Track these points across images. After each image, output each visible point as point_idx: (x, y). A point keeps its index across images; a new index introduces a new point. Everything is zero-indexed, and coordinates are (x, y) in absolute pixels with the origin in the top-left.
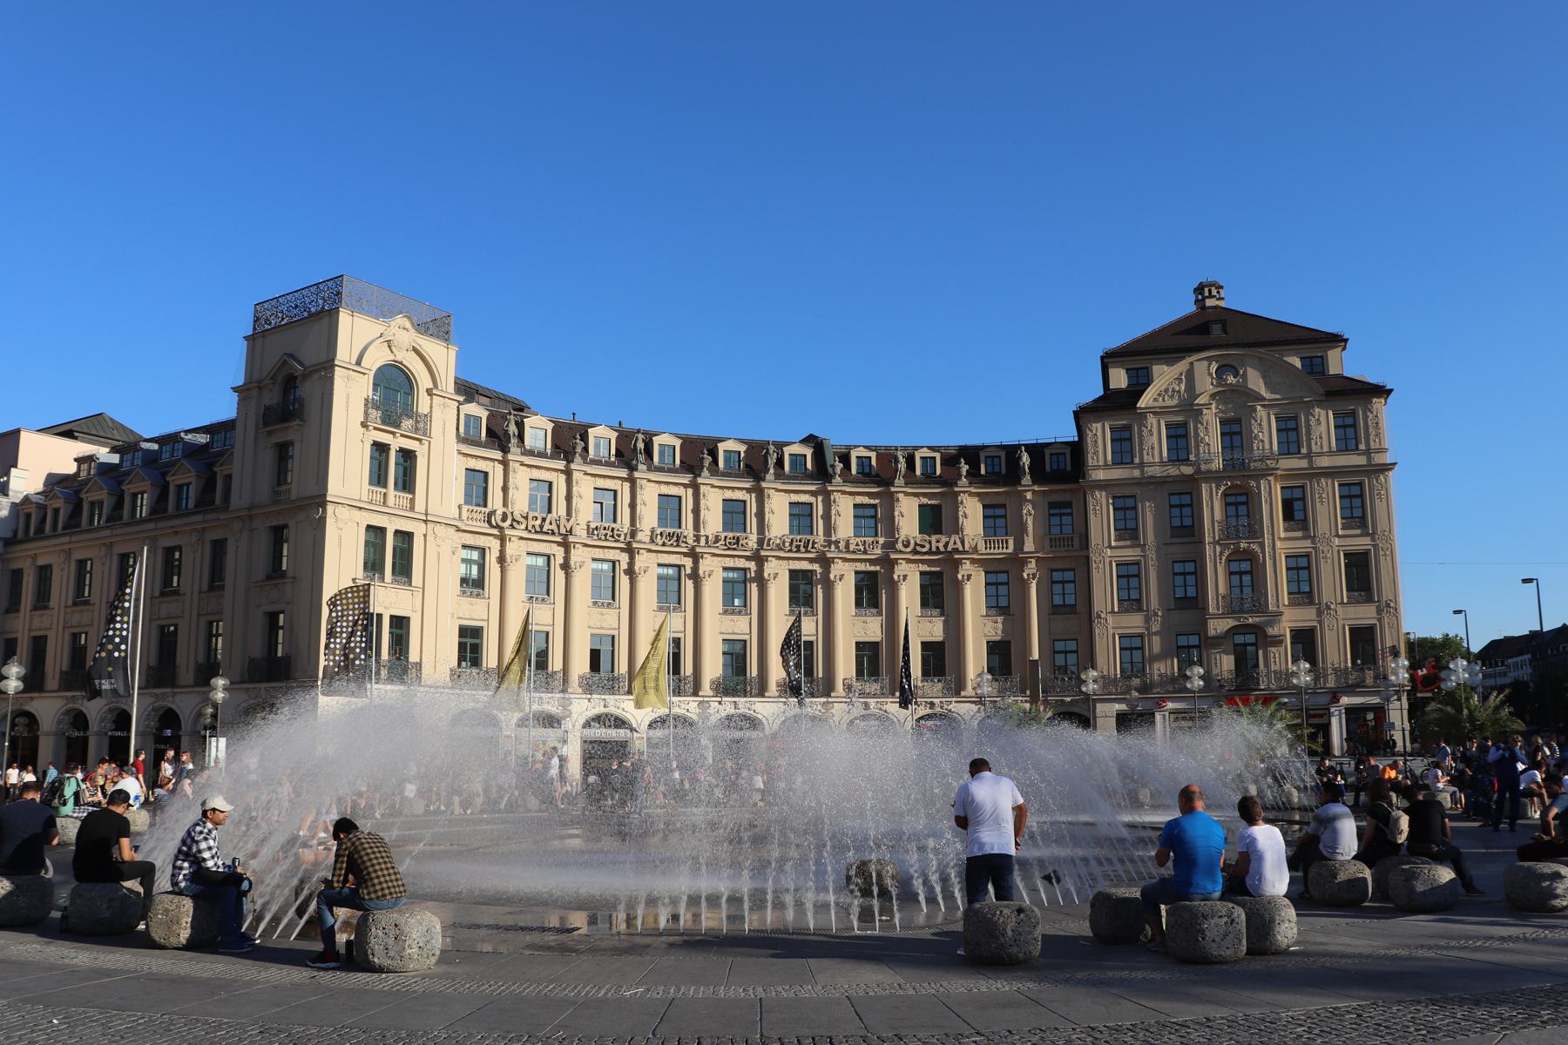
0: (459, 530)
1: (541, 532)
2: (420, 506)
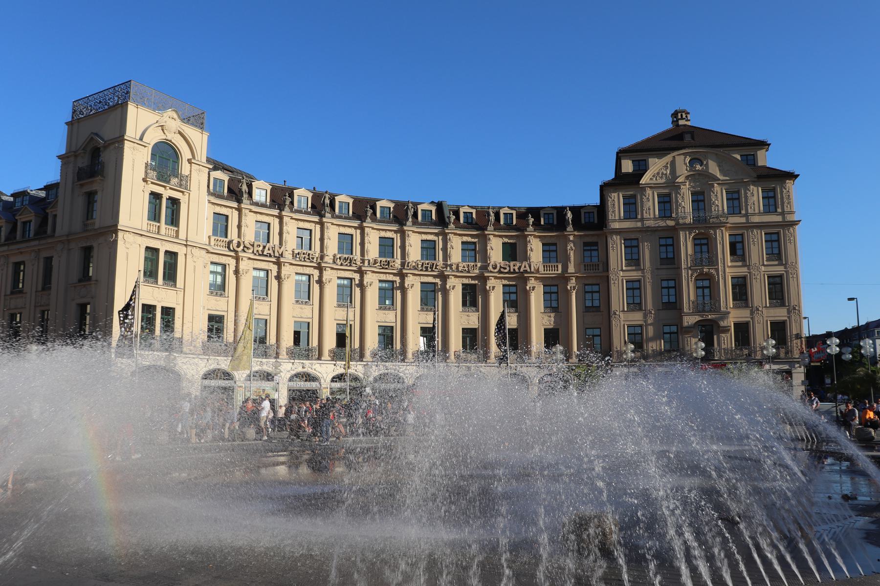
0: (208, 252)
1: (263, 255)
2: (182, 235)
